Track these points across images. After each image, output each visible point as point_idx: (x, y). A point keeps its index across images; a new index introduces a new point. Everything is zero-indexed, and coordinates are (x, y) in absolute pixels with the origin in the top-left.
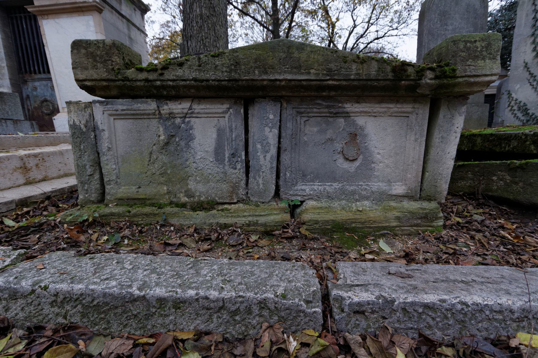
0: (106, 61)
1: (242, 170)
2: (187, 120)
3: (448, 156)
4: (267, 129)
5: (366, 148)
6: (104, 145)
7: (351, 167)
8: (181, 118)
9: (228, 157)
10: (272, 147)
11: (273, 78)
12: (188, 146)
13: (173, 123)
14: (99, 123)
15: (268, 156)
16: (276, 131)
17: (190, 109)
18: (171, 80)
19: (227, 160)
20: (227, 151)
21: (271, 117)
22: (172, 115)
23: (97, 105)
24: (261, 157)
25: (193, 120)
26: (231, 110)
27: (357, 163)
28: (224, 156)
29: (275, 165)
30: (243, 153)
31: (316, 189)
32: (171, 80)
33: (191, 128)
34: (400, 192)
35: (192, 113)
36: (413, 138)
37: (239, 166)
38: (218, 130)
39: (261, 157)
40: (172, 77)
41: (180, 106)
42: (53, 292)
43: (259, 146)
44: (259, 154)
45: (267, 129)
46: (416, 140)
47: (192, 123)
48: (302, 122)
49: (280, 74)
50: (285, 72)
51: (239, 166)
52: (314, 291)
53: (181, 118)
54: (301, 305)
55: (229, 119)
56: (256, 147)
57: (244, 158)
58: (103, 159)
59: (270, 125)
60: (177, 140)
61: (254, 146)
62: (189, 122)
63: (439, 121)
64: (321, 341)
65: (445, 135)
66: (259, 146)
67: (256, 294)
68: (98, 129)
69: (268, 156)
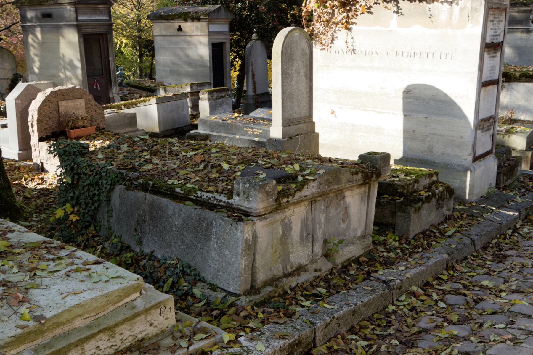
4: (321, 215)
21: (323, 207)
43: (318, 226)
66: (318, 226)
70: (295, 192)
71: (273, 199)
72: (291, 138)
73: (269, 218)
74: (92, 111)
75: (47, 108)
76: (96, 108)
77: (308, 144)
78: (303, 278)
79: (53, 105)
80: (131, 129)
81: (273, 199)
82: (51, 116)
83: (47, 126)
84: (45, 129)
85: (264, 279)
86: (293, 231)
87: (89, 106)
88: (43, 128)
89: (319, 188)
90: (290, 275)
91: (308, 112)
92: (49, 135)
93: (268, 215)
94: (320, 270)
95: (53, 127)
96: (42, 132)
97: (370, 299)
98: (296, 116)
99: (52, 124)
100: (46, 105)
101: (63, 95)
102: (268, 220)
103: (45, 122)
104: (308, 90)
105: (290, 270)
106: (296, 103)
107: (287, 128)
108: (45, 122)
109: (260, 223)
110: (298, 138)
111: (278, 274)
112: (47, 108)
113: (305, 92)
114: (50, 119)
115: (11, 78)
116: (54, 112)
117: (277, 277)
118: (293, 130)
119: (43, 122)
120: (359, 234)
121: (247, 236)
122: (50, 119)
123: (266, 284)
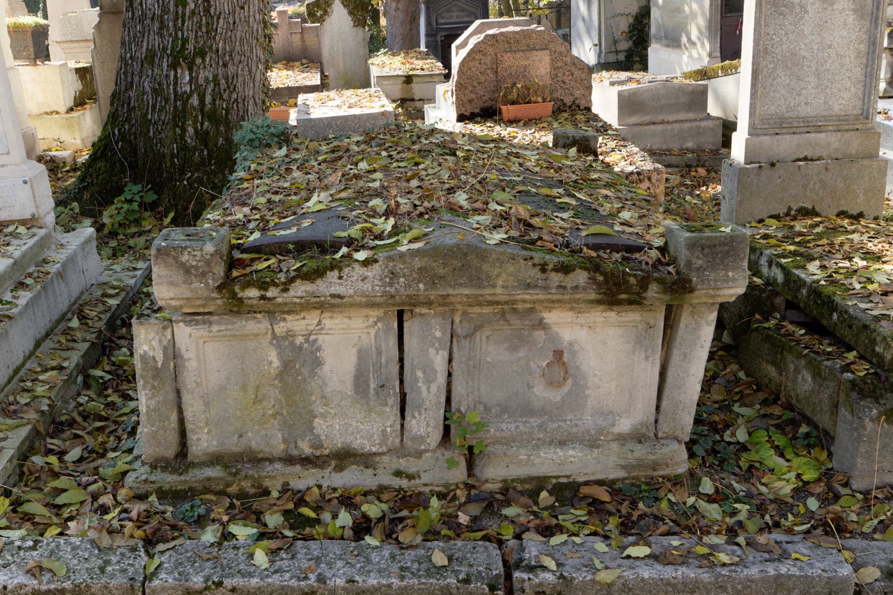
0: (204, 274)
1: (395, 408)
2: (312, 337)
3: (692, 379)
4: (432, 351)
5: (578, 368)
6: (189, 379)
7: (555, 396)
8: (303, 336)
9: (374, 389)
10: (439, 375)
11: (444, 293)
12: (313, 374)
13: (292, 343)
14: (183, 350)
15: (434, 388)
16: (446, 354)
17: (319, 323)
18: (297, 297)
19: (372, 391)
20: (372, 380)
21: (438, 334)
22: (290, 335)
23: (181, 324)
24: (424, 388)
25: (320, 337)
26: (380, 324)
27: (565, 389)
28: (368, 386)
29: (443, 399)
30: (397, 383)
31: (504, 428)
32: (297, 297)
33: (319, 349)
34: (625, 428)
35: (322, 329)
36: (643, 356)
37: (391, 401)
38: (360, 351)
39: (424, 388)
40: (299, 294)
41: (303, 322)
42: (229, 587)
43: (420, 374)
44: (420, 384)
45: (432, 351)
46: (647, 358)
47: (320, 342)
48: (484, 338)
49: (453, 287)
50: (461, 285)
51: (391, 401)
52: (497, 575)
53: (303, 336)
54: (484, 589)
55: (375, 336)
56: (415, 374)
57: (398, 390)
58: (186, 398)
59: (437, 345)
60: (297, 367)
61: (413, 374)
62: (315, 341)
63: (679, 333)
64: (193, 271)
65: (688, 351)
66: (420, 374)
67: (438, 580)
68: (182, 357)
69: (434, 388)
70: (292, 280)
71: (207, 284)
72: (773, 165)
73: (219, 323)
74: (564, 74)
75: (476, 63)
76: (573, 69)
77: (841, 185)
78: (352, 478)
79: (488, 60)
80: (691, 115)
81: (207, 284)
82: (483, 79)
83: (473, 96)
84: (470, 101)
85: (212, 449)
86: (326, 368)
87: (559, 65)
88: (465, 99)
89: (391, 284)
90: (307, 461)
91: (859, 104)
92: (476, 111)
93: (216, 318)
94: (410, 477)
95: (484, 98)
96: (463, 105)
97: (389, 586)
98: (805, 111)
99: (482, 93)
100: (474, 58)
101: (508, 43)
102: (215, 328)
103: (470, 89)
104: (863, 47)
105: (306, 448)
106: (812, 79)
107: (766, 139)
108: (470, 89)
109: (188, 330)
110: (799, 166)
111: (267, 450)
112: (476, 63)
113: (852, 53)
114: (479, 83)
115: (634, 13)
116: (488, 71)
117: (260, 456)
118: (786, 145)
119: (466, 88)
120: (625, 425)
121: (145, 348)
122: (479, 83)
123: (216, 459)
